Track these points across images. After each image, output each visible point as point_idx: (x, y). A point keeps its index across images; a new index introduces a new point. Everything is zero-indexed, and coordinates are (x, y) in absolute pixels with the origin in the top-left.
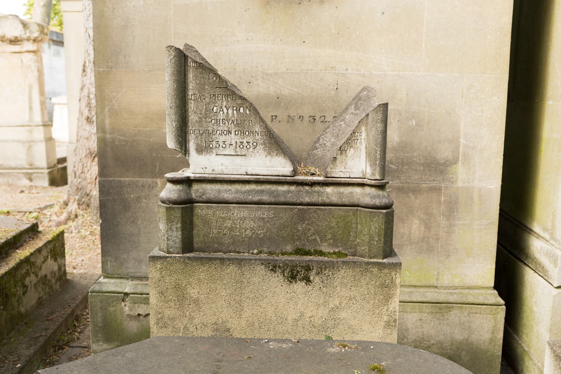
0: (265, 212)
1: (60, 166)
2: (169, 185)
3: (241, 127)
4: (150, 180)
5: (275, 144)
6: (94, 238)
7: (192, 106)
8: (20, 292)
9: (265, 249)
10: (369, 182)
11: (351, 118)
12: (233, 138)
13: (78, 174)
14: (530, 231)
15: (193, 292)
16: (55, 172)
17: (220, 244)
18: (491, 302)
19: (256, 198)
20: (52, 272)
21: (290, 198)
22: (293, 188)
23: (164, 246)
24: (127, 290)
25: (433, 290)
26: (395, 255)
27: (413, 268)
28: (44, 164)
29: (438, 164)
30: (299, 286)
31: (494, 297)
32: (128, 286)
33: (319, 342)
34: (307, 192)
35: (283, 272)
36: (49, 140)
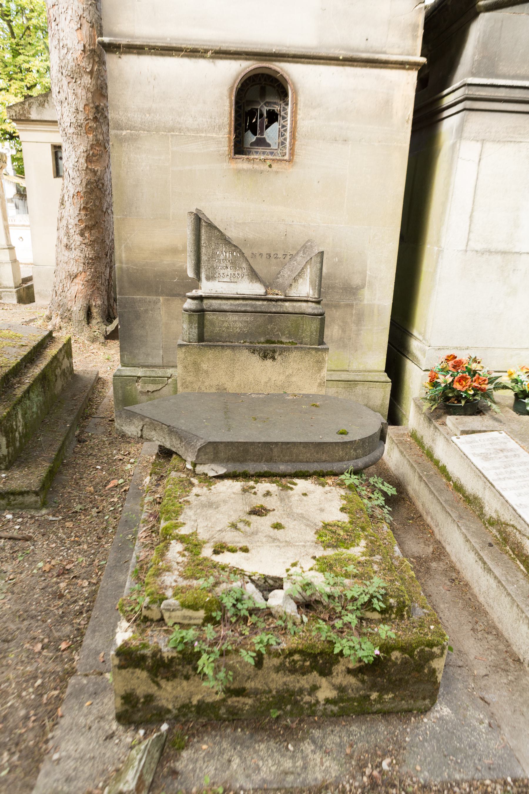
0: (248, 318)
1: (25, 286)
2: (189, 300)
3: (234, 264)
4: (154, 298)
5: (254, 275)
6: (78, 345)
7: (203, 250)
8: (54, 380)
9: (248, 340)
10: (311, 299)
11: (301, 259)
12: (229, 271)
13: (58, 293)
14: (411, 335)
15: (204, 366)
16: (22, 291)
17: (221, 337)
18: (382, 380)
19: (243, 309)
20: (67, 367)
21: (263, 309)
22: (265, 303)
23: (186, 338)
24: (139, 375)
25: (345, 373)
26: (325, 344)
27: (333, 359)
28: (12, 284)
29: (352, 288)
30: (269, 362)
31: (385, 377)
32: (140, 372)
33: (280, 394)
34: (274, 305)
35: (259, 354)
36: (14, 261)
